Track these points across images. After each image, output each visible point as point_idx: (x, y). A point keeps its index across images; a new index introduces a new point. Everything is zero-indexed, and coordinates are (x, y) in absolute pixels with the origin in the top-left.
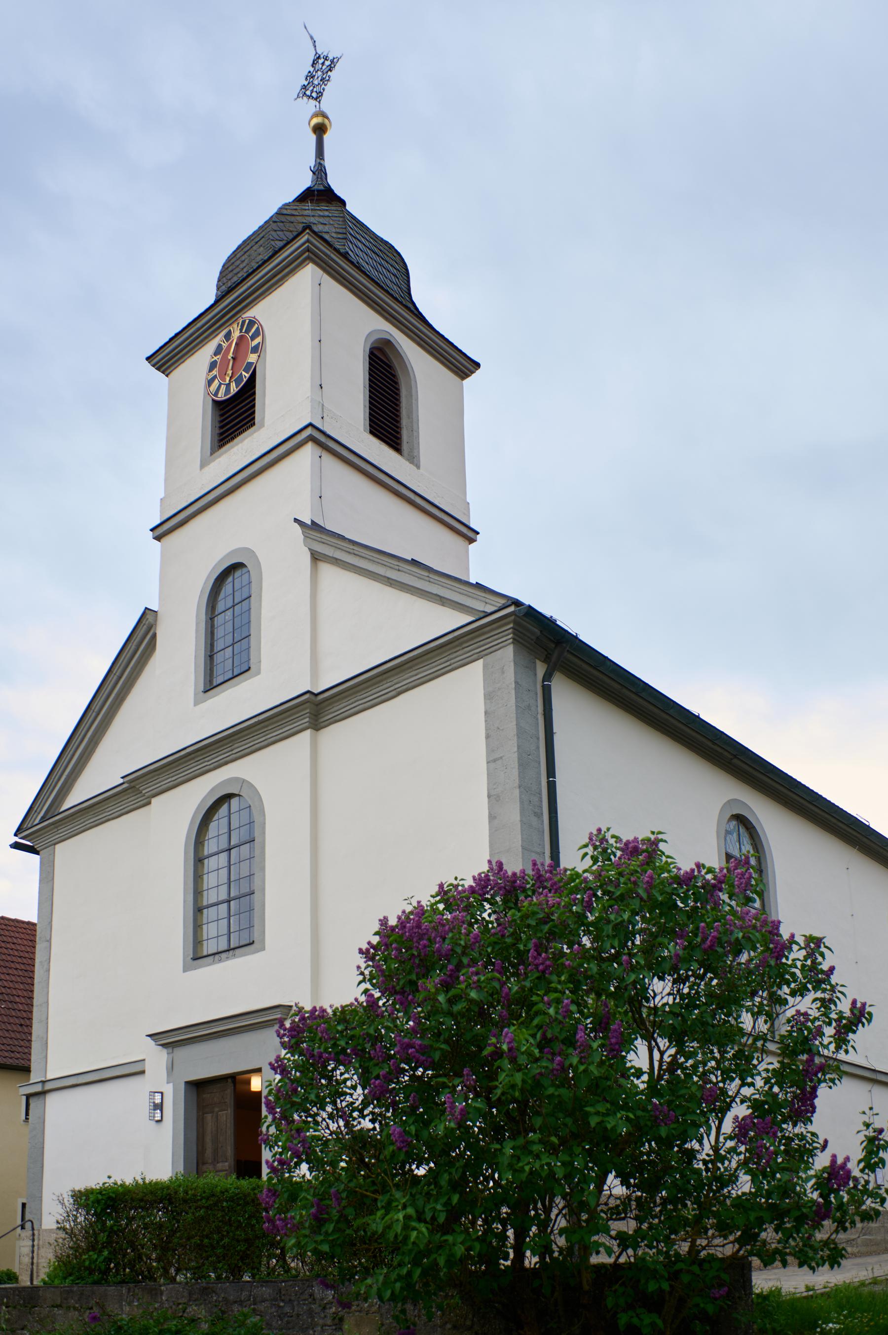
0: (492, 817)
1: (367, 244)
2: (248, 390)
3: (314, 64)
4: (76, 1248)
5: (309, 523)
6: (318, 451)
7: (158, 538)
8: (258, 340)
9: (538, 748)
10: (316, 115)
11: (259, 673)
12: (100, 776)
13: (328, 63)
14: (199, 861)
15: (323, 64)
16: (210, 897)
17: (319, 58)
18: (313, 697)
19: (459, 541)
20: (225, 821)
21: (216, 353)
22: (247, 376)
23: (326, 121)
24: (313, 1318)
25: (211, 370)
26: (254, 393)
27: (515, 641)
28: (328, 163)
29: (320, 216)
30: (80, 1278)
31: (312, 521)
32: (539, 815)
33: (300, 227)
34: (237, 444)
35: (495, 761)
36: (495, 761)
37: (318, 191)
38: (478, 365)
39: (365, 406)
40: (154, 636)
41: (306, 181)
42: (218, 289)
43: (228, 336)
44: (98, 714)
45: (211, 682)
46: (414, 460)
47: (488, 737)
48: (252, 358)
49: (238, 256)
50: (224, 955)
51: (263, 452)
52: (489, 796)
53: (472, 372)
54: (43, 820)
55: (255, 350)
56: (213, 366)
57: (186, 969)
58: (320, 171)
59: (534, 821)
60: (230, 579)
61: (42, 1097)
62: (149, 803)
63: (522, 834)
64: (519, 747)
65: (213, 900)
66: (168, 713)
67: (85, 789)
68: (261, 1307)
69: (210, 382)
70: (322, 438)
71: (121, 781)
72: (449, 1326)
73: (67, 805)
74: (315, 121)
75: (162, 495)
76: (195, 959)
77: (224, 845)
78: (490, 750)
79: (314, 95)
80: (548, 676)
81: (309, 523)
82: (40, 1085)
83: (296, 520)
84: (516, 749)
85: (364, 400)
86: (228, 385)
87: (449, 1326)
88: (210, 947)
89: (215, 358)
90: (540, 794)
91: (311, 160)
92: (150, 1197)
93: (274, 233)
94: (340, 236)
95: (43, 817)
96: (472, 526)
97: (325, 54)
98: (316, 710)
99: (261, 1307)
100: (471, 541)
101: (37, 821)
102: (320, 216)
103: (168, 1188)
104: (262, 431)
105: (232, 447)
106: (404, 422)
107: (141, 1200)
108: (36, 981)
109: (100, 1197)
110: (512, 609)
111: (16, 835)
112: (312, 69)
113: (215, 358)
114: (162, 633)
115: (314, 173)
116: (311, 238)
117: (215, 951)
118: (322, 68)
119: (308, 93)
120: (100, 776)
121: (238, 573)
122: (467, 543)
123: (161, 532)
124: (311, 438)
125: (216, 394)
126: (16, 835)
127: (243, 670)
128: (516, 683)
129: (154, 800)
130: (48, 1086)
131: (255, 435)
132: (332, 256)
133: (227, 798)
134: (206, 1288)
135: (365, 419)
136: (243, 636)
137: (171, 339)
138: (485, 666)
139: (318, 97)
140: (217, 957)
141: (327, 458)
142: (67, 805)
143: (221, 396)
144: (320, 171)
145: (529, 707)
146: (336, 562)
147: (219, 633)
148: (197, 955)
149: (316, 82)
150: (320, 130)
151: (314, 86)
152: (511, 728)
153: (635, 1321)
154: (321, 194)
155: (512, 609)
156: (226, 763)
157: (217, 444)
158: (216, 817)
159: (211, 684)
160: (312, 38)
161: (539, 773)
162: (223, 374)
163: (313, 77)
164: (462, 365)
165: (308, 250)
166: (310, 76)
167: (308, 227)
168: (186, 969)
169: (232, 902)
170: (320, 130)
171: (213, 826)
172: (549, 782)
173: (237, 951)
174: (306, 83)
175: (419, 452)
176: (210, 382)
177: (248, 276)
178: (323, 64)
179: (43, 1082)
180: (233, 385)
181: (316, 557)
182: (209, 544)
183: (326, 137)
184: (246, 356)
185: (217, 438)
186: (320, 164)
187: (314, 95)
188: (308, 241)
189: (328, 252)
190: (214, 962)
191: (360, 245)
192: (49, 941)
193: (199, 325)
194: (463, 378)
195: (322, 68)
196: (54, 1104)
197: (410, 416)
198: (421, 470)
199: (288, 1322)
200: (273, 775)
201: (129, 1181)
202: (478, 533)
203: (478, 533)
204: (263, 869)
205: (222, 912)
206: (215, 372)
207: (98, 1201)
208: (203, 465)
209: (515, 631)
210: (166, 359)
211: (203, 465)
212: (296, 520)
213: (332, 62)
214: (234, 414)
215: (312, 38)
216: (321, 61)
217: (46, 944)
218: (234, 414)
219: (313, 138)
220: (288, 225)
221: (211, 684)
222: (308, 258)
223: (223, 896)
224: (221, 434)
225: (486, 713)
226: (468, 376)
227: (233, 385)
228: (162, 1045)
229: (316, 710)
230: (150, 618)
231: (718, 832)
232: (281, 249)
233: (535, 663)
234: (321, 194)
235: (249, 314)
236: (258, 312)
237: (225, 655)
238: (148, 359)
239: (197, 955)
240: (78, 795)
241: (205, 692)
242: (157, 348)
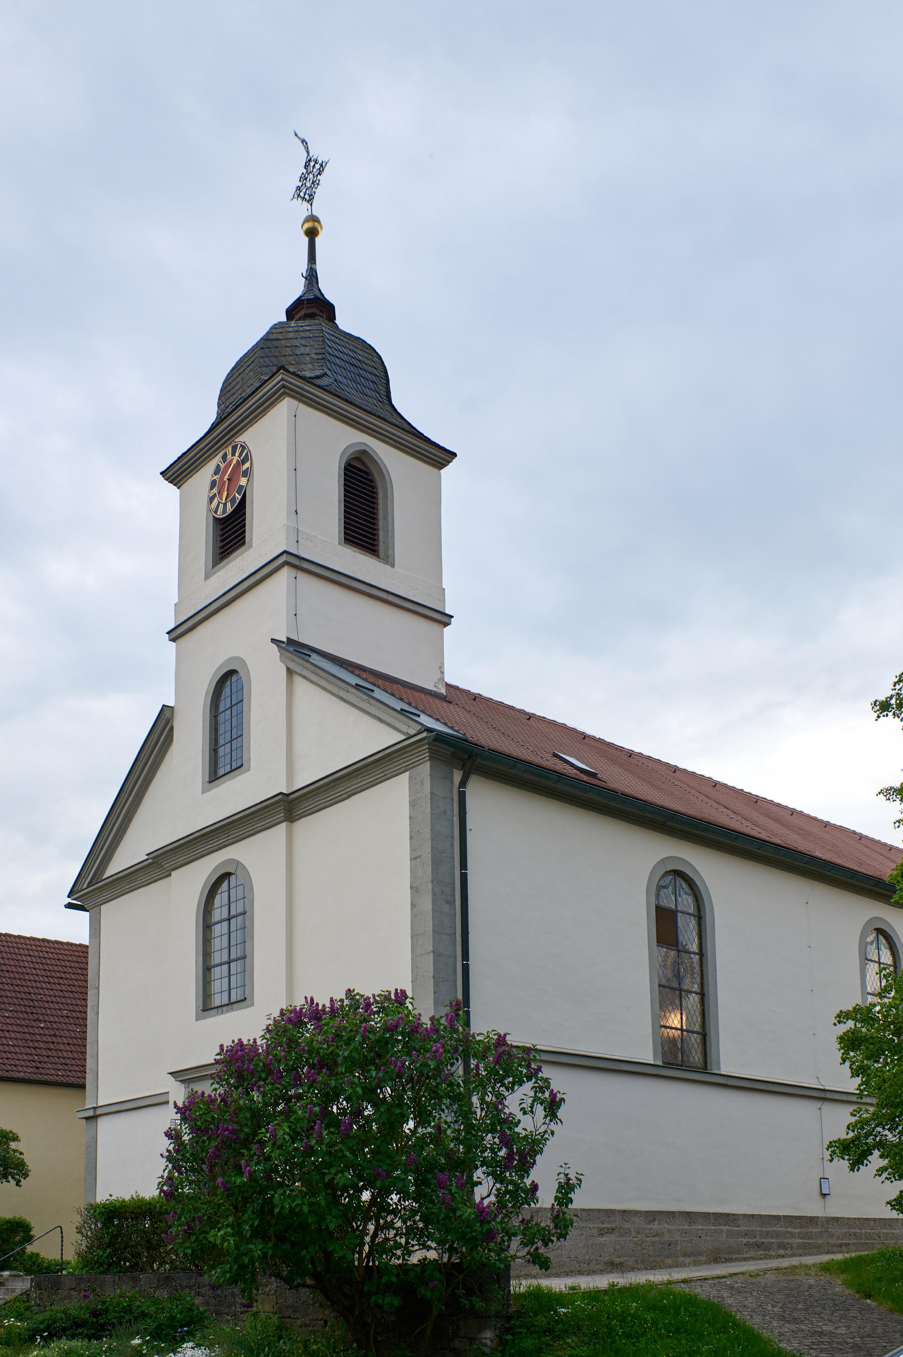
0: (413, 905)
1: (346, 358)
2: (241, 509)
3: (306, 167)
4: (90, 1248)
5: (285, 640)
6: (293, 572)
7: (173, 640)
8: (247, 465)
9: (453, 845)
10: (307, 220)
11: (249, 770)
12: (128, 855)
13: (318, 166)
14: (207, 927)
15: (314, 166)
16: (216, 958)
17: (310, 160)
18: (285, 797)
19: (435, 627)
20: (225, 895)
21: (216, 473)
22: (240, 497)
23: (316, 224)
24: (234, 1298)
25: (212, 489)
26: (245, 514)
27: (431, 758)
28: (319, 267)
29: (302, 338)
30: (92, 1269)
31: (288, 638)
32: (452, 903)
33: (275, 369)
34: (232, 561)
35: (416, 858)
36: (416, 858)
37: (307, 300)
38: (455, 455)
39: (340, 519)
40: (172, 728)
41: (296, 289)
42: (219, 407)
43: (224, 457)
44: (130, 795)
45: (215, 772)
46: (389, 561)
47: (411, 838)
48: (243, 481)
49: (234, 377)
50: (225, 1008)
51: (252, 571)
52: (411, 888)
53: (449, 462)
54: (89, 885)
55: (245, 474)
56: (213, 484)
57: (198, 1018)
58: (312, 277)
59: (446, 908)
60: (228, 683)
61: (94, 1120)
62: (170, 875)
63: (433, 920)
64: (432, 848)
65: (217, 961)
66: (183, 803)
67: (120, 862)
68: (203, 1290)
69: (211, 500)
70: (296, 562)
71: (146, 857)
72: (317, 1305)
73: (107, 875)
74: (307, 226)
75: (176, 601)
76: (204, 1010)
77: (225, 915)
78: (413, 849)
79: (307, 197)
80: (463, 783)
81: (285, 640)
82: (92, 1111)
83: (273, 640)
84: (430, 850)
85: (339, 514)
86: (225, 504)
87: (317, 1305)
88: (217, 1000)
89: (215, 477)
90: (453, 884)
91: (304, 267)
92: (138, 1210)
93: (261, 360)
94: (319, 357)
95: (90, 882)
96: (447, 612)
97: (315, 157)
98: (289, 807)
99: (203, 1290)
100: (446, 624)
101: (85, 886)
102: (302, 338)
103: (150, 1203)
104: (250, 552)
105: (228, 563)
106: (381, 523)
107: (132, 1213)
108: (88, 1022)
109: (103, 1210)
110: (424, 734)
111: (69, 897)
112: (305, 171)
113: (215, 477)
114: (177, 725)
115: (306, 278)
116: (285, 377)
117: (219, 1004)
118: (313, 170)
119: (302, 194)
120: (128, 855)
121: (234, 678)
122: (442, 626)
123: (176, 634)
124: (286, 563)
125: (216, 512)
126: (69, 897)
127: (238, 767)
128: (432, 793)
129: (173, 873)
130: (99, 1112)
131: (245, 554)
132: (306, 387)
133: (227, 875)
134: (168, 1277)
135: (339, 532)
136: (238, 734)
137: (179, 458)
138: (410, 778)
139: (310, 201)
140: (220, 1009)
141: (302, 576)
142: (107, 875)
143: (220, 514)
144: (312, 277)
145: (445, 812)
146: (304, 677)
147: (221, 730)
148: (207, 1007)
149: (308, 185)
150: (312, 234)
151: (306, 191)
152: (427, 833)
153: (380, 1301)
154: (313, 307)
155: (424, 734)
156: (225, 846)
157: (218, 557)
158: (219, 891)
159: (214, 776)
160: (303, 141)
161: (453, 868)
162: (220, 492)
163: (306, 179)
164: (440, 457)
165: (284, 386)
166: (303, 178)
167: (282, 367)
168: (198, 1018)
169: (233, 965)
170: (312, 234)
171: (217, 901)
172: (461, 873)
173: (235, 1005)
174: (300, 184)
175: (394, 551)
176: (211, 500)
177: (245, 395)
178: (314, 166)
179: (95, 1108)
180: (229, 504)
181: (290, 672)
182: (218, 644)
183: (317, 240)
184: (238, 480)
185: (218, 551)
186: (311, 269)
187: (307, 197)
188: (282, 379)
189: (302, 385)
190: (218, 1014)
191: (338, 361)
192: (98, 988)
193: (201, 447)
194: (441, 469)
195: (313, 170)
196: (105, 1126)
197: (386, 518)
198: (396, 568)
199: (219, 1301)
200: (260, 857)
201: (127, 1198)
202: (452, 617)
203: (452, 617)
204: (252, 938)
205: (220, 974)
206: (215, 491)
207: (103, 1213)
208: (207, 577)
209: (431, 750)
210: (177, 473)
211: (207, 577)
212: (273, 640)
213: (321, 165)
214: (230, 533)
215: (303, 141)
216: (312, 164)
217: (95, 991)
218: (230, 533)
219: (307, 239)
220: (273, 350)
221: (214, 776)
222: (284, 393)
223: (225, 959)
224: (222, 547)
225: (410, 817)
226: (445, 466)
227: (229, 504)
228: (181, 1081)
229: (289, 807)
230: (167, 713)
231: (647, 890)
232: (266, 381)
233: (452, 772)
234: (313, 307)
235: (241, 439)
236: (248, 437)
237: (224, 756)
238: (161, 473)
239: (207, 1007)
240: (116, 866)
241: (210, 782)
242: (168, 465)
